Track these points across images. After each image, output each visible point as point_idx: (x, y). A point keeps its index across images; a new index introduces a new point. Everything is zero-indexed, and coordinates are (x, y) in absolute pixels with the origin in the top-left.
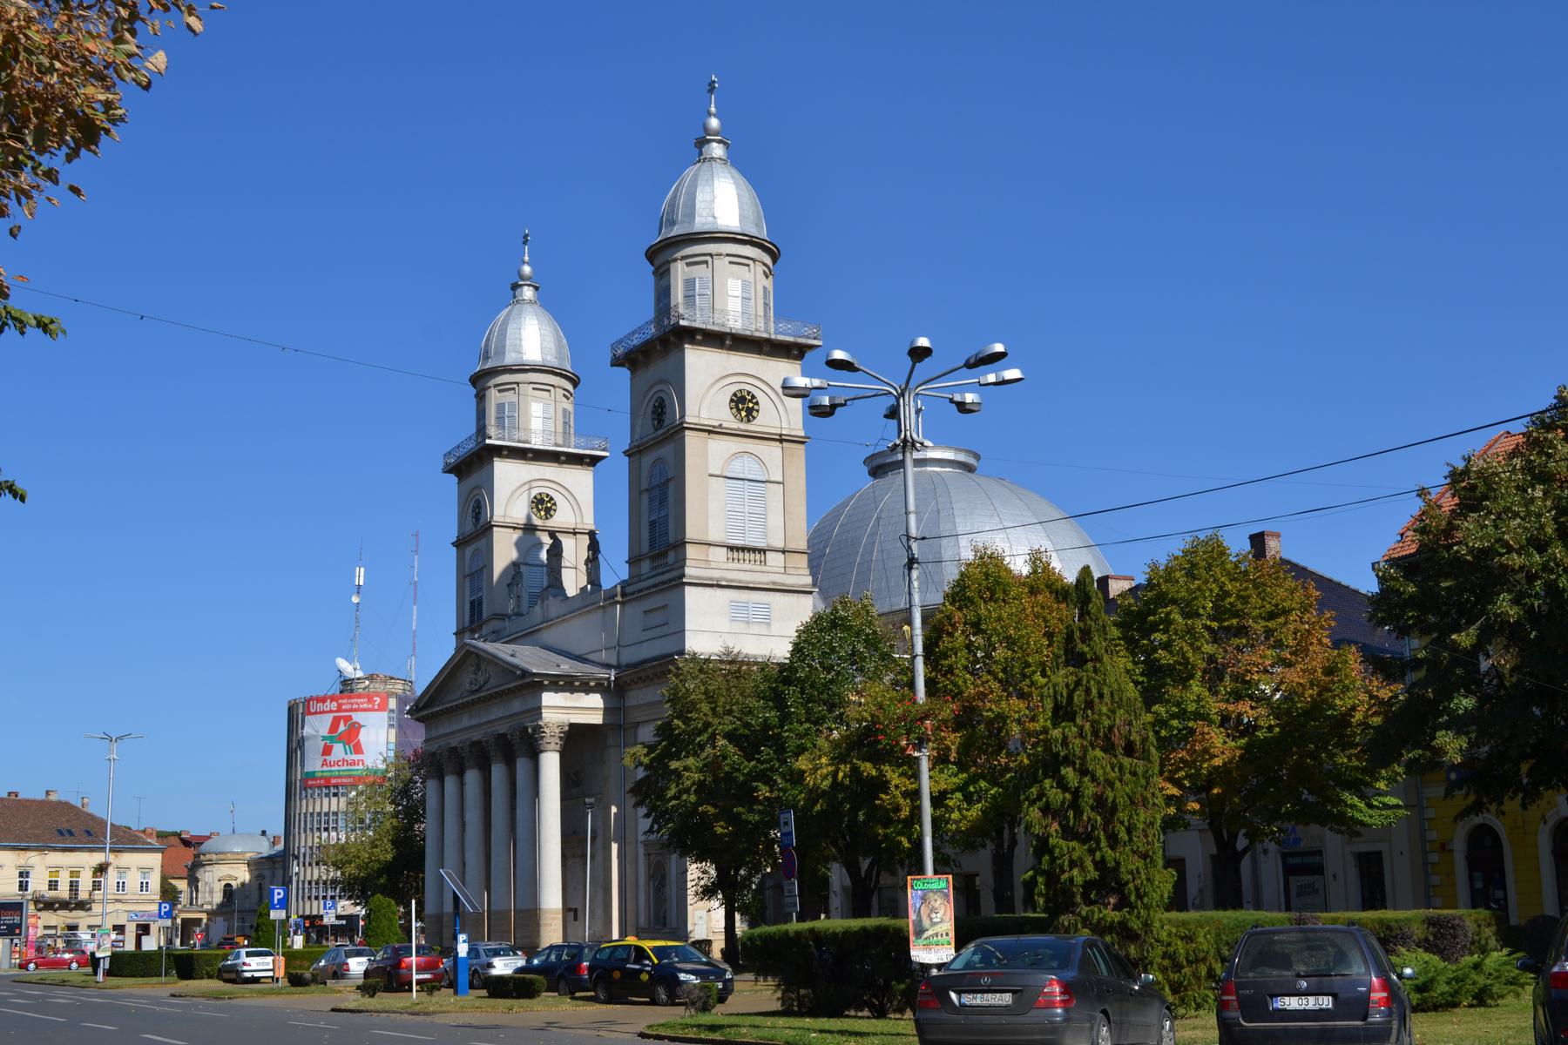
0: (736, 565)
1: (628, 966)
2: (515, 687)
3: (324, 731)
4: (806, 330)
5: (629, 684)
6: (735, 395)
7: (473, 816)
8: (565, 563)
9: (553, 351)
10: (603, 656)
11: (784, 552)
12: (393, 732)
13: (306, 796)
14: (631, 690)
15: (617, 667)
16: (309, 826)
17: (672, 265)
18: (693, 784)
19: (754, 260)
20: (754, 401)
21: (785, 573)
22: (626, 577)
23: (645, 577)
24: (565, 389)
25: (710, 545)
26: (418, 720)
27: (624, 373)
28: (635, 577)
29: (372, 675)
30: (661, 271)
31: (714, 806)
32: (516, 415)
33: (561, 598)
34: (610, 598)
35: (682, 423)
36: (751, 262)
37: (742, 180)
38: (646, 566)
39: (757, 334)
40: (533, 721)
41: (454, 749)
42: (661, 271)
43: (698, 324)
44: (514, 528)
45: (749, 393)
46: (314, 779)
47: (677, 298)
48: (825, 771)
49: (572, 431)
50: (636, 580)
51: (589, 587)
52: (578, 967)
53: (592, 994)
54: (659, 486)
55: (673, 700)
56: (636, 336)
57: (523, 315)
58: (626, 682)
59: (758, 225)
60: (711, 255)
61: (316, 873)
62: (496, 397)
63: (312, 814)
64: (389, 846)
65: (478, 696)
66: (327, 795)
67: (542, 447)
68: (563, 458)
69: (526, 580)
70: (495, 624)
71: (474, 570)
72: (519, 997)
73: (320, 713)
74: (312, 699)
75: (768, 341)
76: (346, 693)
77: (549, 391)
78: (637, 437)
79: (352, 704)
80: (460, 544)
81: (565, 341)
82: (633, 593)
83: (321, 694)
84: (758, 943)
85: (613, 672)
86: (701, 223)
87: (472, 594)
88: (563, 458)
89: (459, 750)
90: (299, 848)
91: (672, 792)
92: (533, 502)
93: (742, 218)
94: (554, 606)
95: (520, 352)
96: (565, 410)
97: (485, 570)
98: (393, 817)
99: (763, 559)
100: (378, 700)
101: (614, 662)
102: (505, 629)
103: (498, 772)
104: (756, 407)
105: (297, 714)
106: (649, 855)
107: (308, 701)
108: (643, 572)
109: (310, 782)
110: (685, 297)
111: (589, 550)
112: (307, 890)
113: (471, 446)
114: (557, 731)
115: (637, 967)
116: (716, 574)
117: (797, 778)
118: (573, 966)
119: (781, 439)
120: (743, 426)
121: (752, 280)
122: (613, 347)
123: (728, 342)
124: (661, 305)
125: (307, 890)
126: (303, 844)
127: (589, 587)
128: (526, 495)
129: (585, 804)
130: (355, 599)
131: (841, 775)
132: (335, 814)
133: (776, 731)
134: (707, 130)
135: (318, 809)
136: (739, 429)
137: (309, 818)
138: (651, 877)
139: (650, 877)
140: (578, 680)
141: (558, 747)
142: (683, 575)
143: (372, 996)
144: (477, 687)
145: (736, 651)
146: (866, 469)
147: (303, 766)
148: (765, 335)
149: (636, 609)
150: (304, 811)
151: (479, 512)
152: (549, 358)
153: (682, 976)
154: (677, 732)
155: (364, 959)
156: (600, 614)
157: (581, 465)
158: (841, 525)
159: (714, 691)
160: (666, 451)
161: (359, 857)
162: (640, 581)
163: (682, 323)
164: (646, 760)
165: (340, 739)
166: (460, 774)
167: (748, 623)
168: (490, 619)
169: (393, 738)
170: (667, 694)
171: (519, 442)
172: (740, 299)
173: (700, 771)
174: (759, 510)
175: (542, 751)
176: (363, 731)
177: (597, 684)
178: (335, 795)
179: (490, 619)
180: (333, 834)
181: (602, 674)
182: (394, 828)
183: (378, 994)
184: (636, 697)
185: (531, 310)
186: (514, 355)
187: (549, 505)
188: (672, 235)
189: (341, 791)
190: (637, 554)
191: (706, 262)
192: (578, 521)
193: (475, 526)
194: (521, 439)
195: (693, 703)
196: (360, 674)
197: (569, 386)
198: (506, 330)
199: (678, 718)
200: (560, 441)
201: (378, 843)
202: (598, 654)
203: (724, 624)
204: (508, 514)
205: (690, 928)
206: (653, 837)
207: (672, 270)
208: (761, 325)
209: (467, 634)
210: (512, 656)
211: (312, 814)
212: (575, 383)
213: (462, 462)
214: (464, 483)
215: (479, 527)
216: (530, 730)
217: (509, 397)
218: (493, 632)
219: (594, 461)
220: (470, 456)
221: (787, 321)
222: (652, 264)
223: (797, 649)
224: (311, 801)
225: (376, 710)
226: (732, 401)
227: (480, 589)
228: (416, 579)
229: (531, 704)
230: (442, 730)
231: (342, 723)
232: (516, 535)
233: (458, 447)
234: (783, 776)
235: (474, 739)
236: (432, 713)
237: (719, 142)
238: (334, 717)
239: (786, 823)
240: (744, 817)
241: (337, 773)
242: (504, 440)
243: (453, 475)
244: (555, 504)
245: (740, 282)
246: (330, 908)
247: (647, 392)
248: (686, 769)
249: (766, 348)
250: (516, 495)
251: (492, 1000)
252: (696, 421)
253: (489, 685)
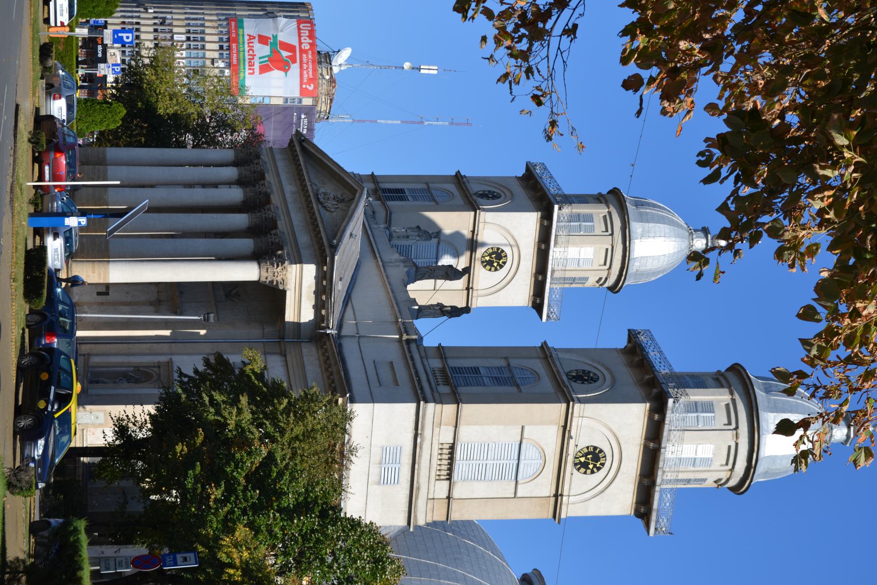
0: (436, 451)
1: (53, 388)
2: (321, 238)
3: (282, 37)
4: (664, 522)
5: (322, 347)
6: (601, 451)
7: (199, 196)
8: (440, 282)
9: (643, 268)
10: (349, 322)
11: (449, 498)
12: (280, 102)
13: (220, 20)
14: (317, 349)
15: (339, 336)
16: (192, 22)
17: (726, 390)
18: (225, 419)
19: (732, 470)
20: (595, 470)
21: (428, 499)
22: (426, 343)
23: (426, 363)
24: (606, 279)
25: (456, 427)
26: (291, 141)
27: (622, 342)
28: (425, 352)
29: (334, 82)
30: (721, 379)
31: (203, 444)
32: (582, 233)
33: (406, 278)
34: (405, 328)
35: (573, 401)
36: (730, 466)
38: (436, 363)
39: (660, 473)
40: (288, 254)
41: (262, 176)
42: (721, 379)
43: (669, 415)
44: (473, 232)
45: (603, 464)
46: (236, 28)
47: (695, 395)
48: (235, 556)
49: (567, 286)
50: (423, 354)
51: (417, 307)
52: (52, 333)
53: (27, 350)
54: (513, 377)
55: (309, 398)
56: (658, 355)
57: (678, 239)
58: (325, 344)
59: (766, 473)
60: (737, 428)
61: (147, 37)
62: (598, 214)
63: (203, 25)
64: (171, 111)
65: (313, 201)
66: (221, 40)
67: (550, 257)
68: (540, 278)
69: (423, 244)
70: (381, 214)
71: (433, 192)
72: (26, 282)
73: (299, 33)
74: (313, 25)
75: (653, 484)
76: (317, 57)
77: (605, 264)
78: (561, 355)
79: (307, 64)
80: (458, 179)
81: (653, 279)
82: (410, 352)
83: (317, 34)
84: (72, 539)
85: (334, 332)
87: (412, 190)
88: (540, 278)
89: (262, 182)
90: (171, 13)
91: (218, 397)
92: (498, 249)
93: (774, 458)
94: (398, 272)
95: (642, 236)
96: (587, 279)
97: (433, 203)
98: (198, 114)
99: (442, 477)
100: (311, 88)
101: (344, 332)
102: (377, 224)
103: (241, 220)
104: (589, 471)
105: (298, 12)
106: (159, 367)
107: (310, 21)
108: (429, 360)
109: (233, 24)
110: (696, 403)
111: (452, 307)
112: (130, 20)
113: (552, 191)
114: (279, 279)
115: (51, 397)
116: (427, 433)
117: (228, 528)
118: (53, 329)
119: (557, 496)
120: (570, 459)
121: (712, 468)
122: (647, 332)
123: (652, 445)
124: (688, 379)
125: (130, 20)
126: (175, 16)
127: (417, 307)
128: (505, 242)
129: (208, 314)
130: (407, 65)
131: (231, 571)
132: (203, 48)
133: (275, 504)
135: (207, 31)
136: (567, 455)
137: (199, 22)
138: (137, 368)
139: (138, 367)
140: (327, 298)
141: (263, 279)
142: (426, 402)
143: (29, 141)
144: (322, 200)
145: (353, 458)
146: (528, 570)
147: (249, 16)
148: (659, 481)
149: (394, 354)
150: (206, 18)
151: (488, 198)
152: (637, 264)
153: (41, 442)
154: (276, 401)
155: (65, 118)
156: (391, 318)
157: (534, 295)
158: (474, 548)
159: (315, 438)
160: (547, 384)
161: (161, 83)
162: (421, 358)
163: (671, 401)
164: (248, 369)
165: (274, 52)
166: (240, 182)
167: (381, 463)
168: (386, 209)
169: (274, 101)
170: (312, 392)
171: (556, 236)
173: (238, 425)
174: (489, 474)
175: (259, 264)
176: (282, 73)
177: (323, 316)
178: (221, 48)
179: (386, 209)
180: (184, 54)
181: (333, 322)
182: (189, 116)
183: (31, 145)
184: (310, 355)
185: (683, 247)
186: (639, 230)
187: (495, 264)
188: (756, 390)
189: (225, 53)
190: (448, 355)
191: (730, 423)
192: (480, 292)
193: (475, 194)
194: (559, 238)
195: (303, 418)
196: (336, 70)
197: (610, 282)
198: (664, 223)
199: (289, 403)
200: (557, 275)
201: (174, 101)
202: (352, 316)
203: (379, 440)
204: (487, 226)
205: (88, 407)
206: (176, 376)
207: (721, 390)
208: (669, 476)
209: (371, 186)
210: (351, 235)
211: (203, 25)
212: (612, 289)
213: (537, 182)
214: (516, 182)
215: (475, 197)
216: (280, 252)
217: (599, 227)
218: (374, 212)
219: (538, 307)
220: (542, 187)
221: (673, 503)
222: (728, 370)
223: (355, 524)
224: (215, 24)
225: (301, 86)
226: (595, 448)
227: (415, 198)
228: (426, 123)
229: (305, 253)
230: (281, 164)
231: (290, 54)
232: (467, 233)
233: (551, 177)
234: (231, 512)
235: (272, 196)
236: (297, 155)
237: (848, 436)
238: (295, 47)
239: (185, 559)
240: (190, 472)
241: (241, 49)
242: (558, 222)
243: (524, 171)
244: (496, 270)
245: (711, 456)
246: (113, 69)
247: (603, 365)
248: (240, 411)
249: (646, 482)
250: (503, 231)
251: (23, 254)
252: (575, 414)
253: (322, 211)
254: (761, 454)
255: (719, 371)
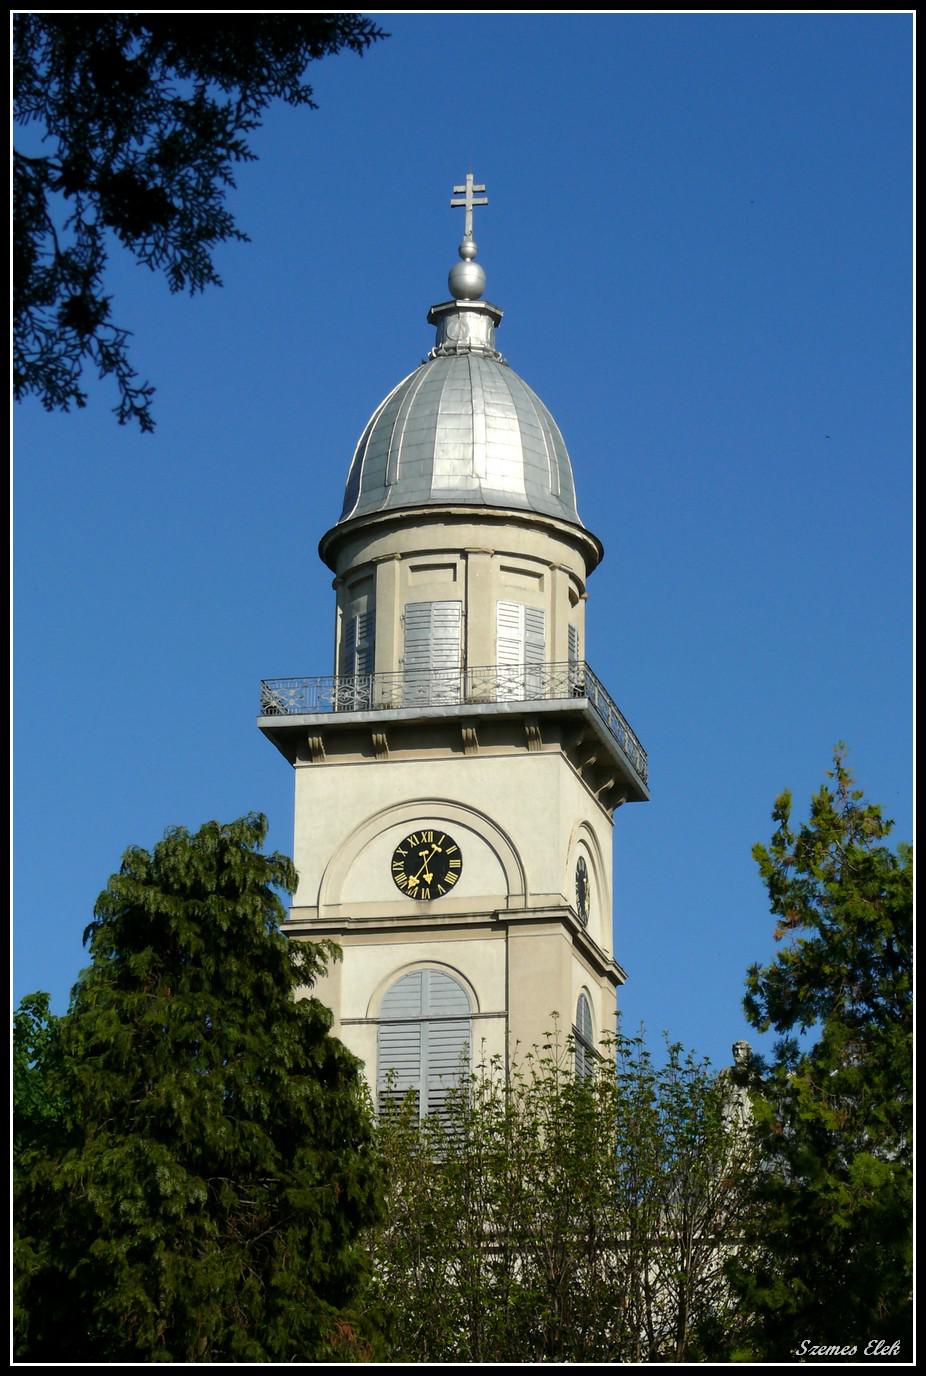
37: (529, 395)
86: (448, 476)
134: (458, 293)
172: (521, 646)
252: (311, 915)
254: (523, 501)
255: (335, 585)
